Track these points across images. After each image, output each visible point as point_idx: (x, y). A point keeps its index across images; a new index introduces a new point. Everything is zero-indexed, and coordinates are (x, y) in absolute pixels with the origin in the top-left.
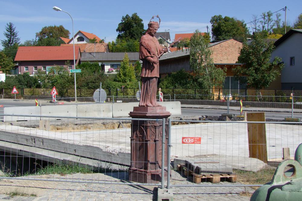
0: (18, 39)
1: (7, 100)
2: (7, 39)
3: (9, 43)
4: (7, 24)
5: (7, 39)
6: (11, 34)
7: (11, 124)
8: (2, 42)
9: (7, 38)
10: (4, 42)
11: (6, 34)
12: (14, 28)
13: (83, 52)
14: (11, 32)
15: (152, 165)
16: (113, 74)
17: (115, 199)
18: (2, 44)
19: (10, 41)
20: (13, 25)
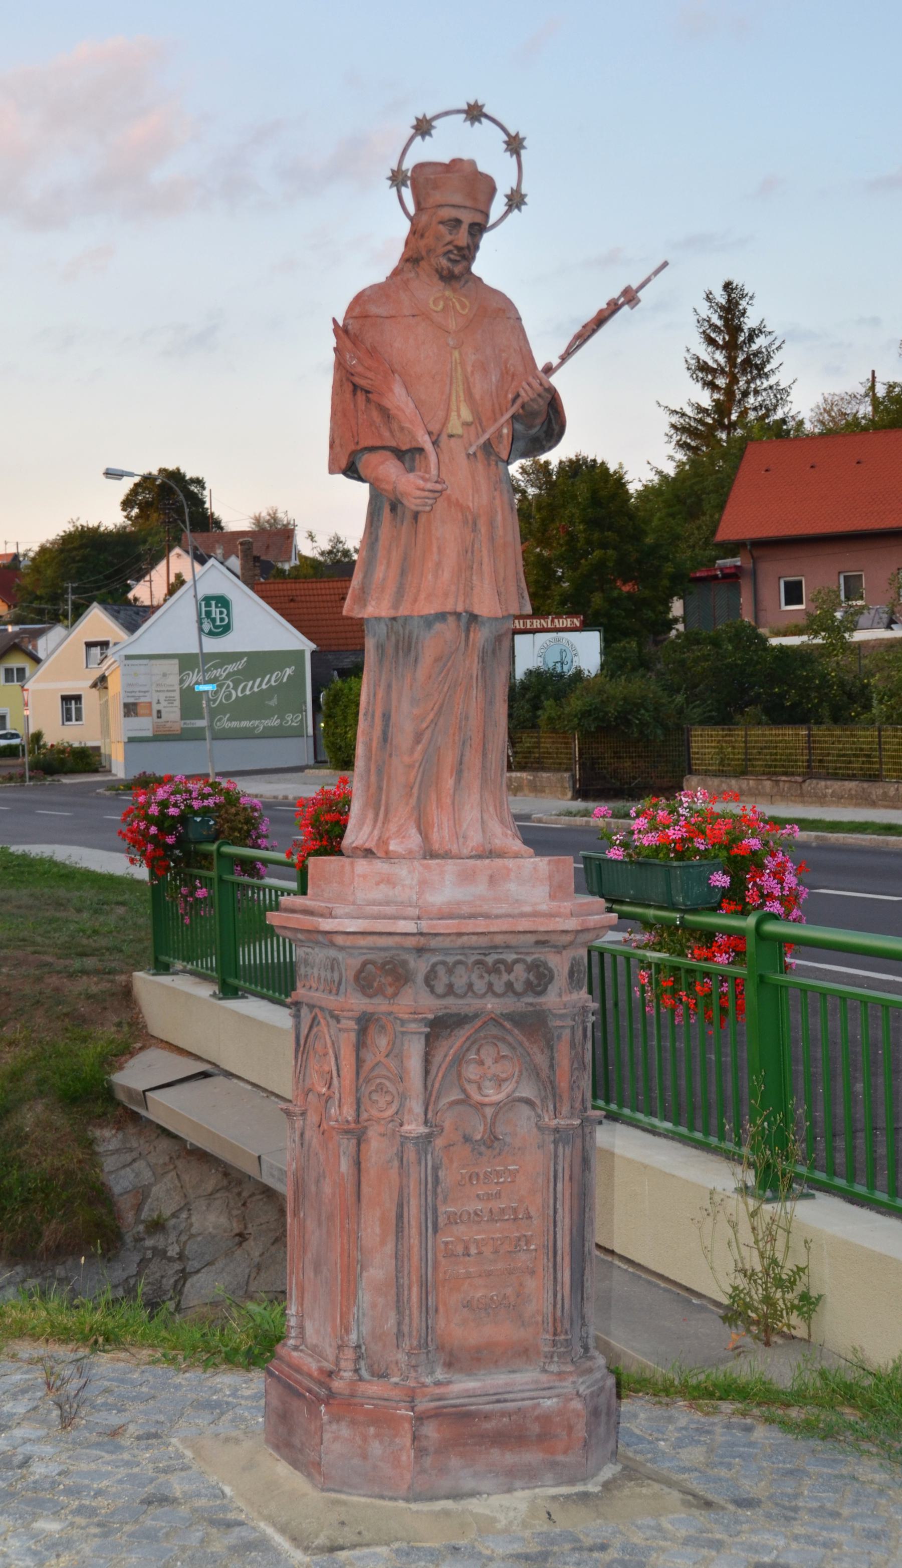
0: (781, 394)
1: (343, 1063)
2: (706, 399)
3: (719, 424)
4: (709, 298)
5: (706, 399)
6: (731, 360)
7: (456, 1549)
8: (675, 419)
9: (707, 393)
10: (763, 365)
11: (703, 367)
12: (750, 322)
13: (541, 659)
14: (731, 347)
15: (149, 895)
16: (52, 862)
17: (832, 1535)
18: (676, 438)
19: (721, 408)
20: (743, 303)
